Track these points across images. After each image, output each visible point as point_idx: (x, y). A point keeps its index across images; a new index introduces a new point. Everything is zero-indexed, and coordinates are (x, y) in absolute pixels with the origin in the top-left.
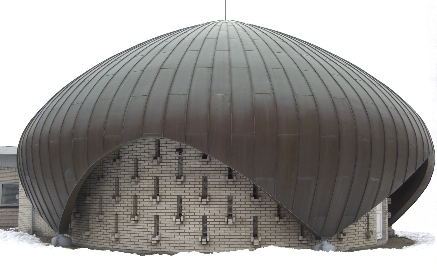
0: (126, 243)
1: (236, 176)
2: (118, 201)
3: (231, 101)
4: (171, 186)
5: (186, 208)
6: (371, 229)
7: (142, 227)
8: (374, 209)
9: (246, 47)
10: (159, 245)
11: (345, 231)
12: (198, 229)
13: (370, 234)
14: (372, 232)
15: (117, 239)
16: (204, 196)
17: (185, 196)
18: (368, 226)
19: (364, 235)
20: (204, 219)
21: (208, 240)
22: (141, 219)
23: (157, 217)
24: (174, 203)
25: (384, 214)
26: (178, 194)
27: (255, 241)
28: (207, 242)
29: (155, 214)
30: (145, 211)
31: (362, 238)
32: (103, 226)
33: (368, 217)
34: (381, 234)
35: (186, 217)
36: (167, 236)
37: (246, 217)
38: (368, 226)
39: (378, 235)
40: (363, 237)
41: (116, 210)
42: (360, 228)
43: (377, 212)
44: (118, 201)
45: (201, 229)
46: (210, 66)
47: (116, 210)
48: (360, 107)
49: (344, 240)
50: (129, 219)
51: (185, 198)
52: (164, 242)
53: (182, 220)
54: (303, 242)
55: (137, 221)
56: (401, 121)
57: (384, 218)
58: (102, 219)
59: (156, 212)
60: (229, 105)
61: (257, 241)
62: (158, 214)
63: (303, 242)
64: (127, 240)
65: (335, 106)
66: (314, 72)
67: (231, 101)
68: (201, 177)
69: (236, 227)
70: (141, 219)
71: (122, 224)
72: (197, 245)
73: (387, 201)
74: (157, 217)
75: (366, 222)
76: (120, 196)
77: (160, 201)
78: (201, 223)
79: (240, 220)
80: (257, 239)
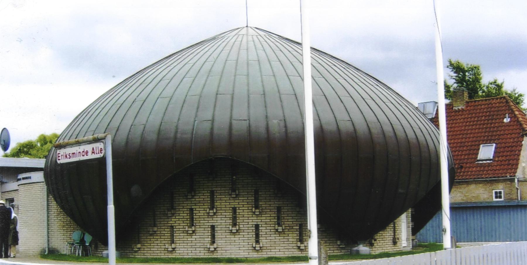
0: (182, 252)
1: (238, 190)
2: (173, 214)
3: (286, 127)
4: (225, 199)
5: (241, 218)
6: (398, 236)
7: (199, 237)
8: (400, 218)
9: (289, 74)
10: (216, 252)
11: (376, 237)
12: (251, 236)
13: (397, 241)
14: (398, 239)
15: (174, 249)
16: (257, 207)
17: (239, 207)
18: (394, 233)
19: (392, 241)
20: (257, 227)
21: (261, 246)
22: (197, 229)
23: (213, 228)
24: (229, 214)
25: (408, 223)
26: (233, 206)
27: (302, 245)
28: (260, 247)
29: (211, 224)
30: (201, 222)
31: (390, 243)
32: (157, 237)
33: (394, 224)
34: (405, 242)
35: (241, 226)
36: (223, 244)
37: (293, 225)
38: (394, 233)
39: (403, 242)
40: (391, 243)
41: (171, 222)
42: (388, 234)
43: (402, 221)
44: (173, 214)
45: (254, 236)
46: (262, 93)
47: (171, 222)
48: (390, 129)
49: (375, 244)
50: (187, 229)
51: (239, 209)
52: (220, 249)
53: (238, 229)
54: (341, 246)
55: (194, 232)
56: (423, 138)
57: (408, 227)
58: (155, 231)
59: (211, 222)
60: (284, 130)
61: (303, 245)
62: (214, 224)
63: (341, 246)
64: (183, 249)
65: (369, 129)
66: (350, 98)
67: (286, 127)
68: (253, 191)
69: (284, 234)
70: (197, 229)
71: (178, 235)
72: (251, 251)
73: (410, 211)
74: (213, 228)
75: (392, 230)
76: (175, 209)
77: (216, 212)
78: (254, 231)
79: (288, 228)
80: (303, 243)
